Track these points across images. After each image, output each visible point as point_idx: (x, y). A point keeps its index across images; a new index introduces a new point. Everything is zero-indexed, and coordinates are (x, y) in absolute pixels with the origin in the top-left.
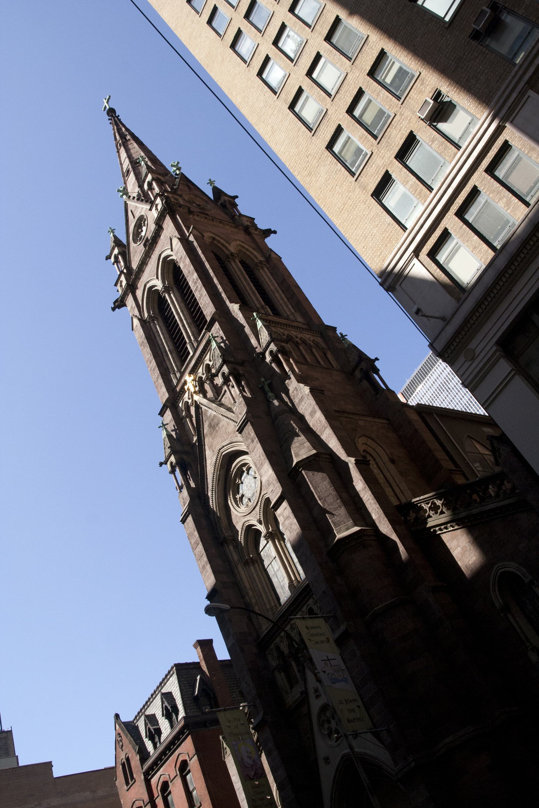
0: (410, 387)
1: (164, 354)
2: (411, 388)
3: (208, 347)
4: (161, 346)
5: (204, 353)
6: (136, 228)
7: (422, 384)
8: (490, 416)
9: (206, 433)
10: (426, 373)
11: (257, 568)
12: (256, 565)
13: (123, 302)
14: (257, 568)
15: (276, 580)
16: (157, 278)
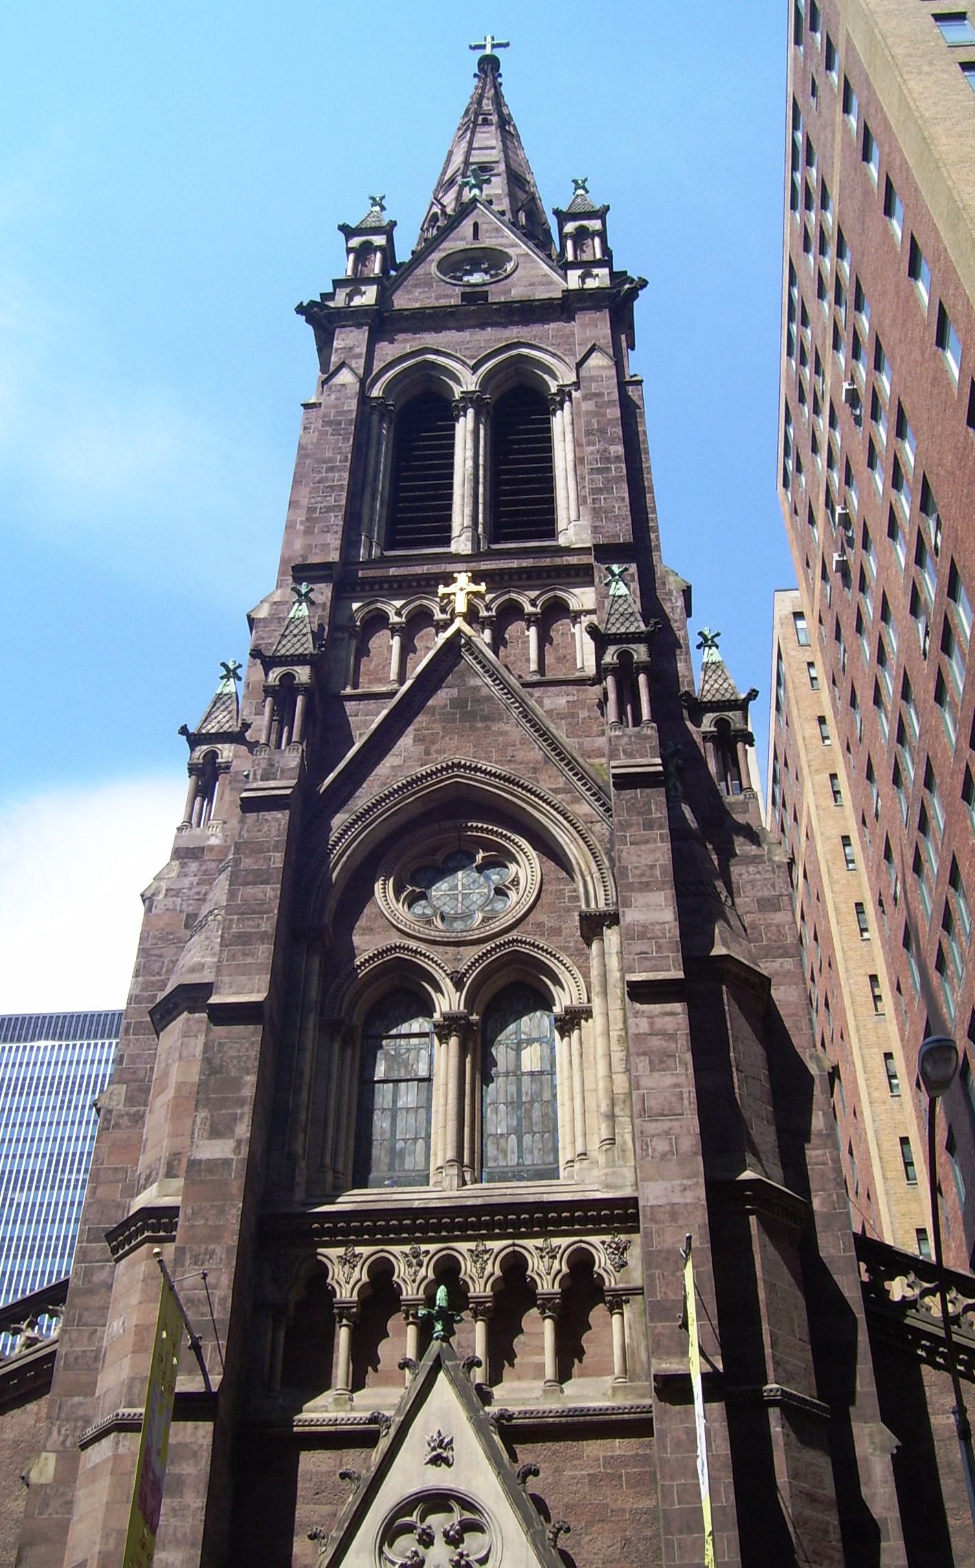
0: (29, 1023)
1: (369, 489)
2: (21, 1029)
3: (549, 577)
4: (371, 470)
5: (529, 578)
6: (463, 255)
7: (57, 1043)
8: (858, 1261)
9: (434, 708)
10: (61, 1034)
11: (349, 1057)
12: (349, 1052)
13: (331, 323)
14: (349, 1057)
15: (386, 1125)
16: (475, 369)
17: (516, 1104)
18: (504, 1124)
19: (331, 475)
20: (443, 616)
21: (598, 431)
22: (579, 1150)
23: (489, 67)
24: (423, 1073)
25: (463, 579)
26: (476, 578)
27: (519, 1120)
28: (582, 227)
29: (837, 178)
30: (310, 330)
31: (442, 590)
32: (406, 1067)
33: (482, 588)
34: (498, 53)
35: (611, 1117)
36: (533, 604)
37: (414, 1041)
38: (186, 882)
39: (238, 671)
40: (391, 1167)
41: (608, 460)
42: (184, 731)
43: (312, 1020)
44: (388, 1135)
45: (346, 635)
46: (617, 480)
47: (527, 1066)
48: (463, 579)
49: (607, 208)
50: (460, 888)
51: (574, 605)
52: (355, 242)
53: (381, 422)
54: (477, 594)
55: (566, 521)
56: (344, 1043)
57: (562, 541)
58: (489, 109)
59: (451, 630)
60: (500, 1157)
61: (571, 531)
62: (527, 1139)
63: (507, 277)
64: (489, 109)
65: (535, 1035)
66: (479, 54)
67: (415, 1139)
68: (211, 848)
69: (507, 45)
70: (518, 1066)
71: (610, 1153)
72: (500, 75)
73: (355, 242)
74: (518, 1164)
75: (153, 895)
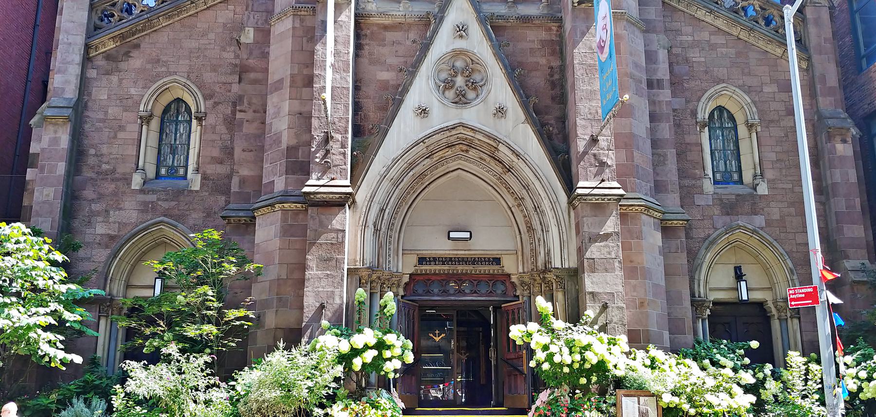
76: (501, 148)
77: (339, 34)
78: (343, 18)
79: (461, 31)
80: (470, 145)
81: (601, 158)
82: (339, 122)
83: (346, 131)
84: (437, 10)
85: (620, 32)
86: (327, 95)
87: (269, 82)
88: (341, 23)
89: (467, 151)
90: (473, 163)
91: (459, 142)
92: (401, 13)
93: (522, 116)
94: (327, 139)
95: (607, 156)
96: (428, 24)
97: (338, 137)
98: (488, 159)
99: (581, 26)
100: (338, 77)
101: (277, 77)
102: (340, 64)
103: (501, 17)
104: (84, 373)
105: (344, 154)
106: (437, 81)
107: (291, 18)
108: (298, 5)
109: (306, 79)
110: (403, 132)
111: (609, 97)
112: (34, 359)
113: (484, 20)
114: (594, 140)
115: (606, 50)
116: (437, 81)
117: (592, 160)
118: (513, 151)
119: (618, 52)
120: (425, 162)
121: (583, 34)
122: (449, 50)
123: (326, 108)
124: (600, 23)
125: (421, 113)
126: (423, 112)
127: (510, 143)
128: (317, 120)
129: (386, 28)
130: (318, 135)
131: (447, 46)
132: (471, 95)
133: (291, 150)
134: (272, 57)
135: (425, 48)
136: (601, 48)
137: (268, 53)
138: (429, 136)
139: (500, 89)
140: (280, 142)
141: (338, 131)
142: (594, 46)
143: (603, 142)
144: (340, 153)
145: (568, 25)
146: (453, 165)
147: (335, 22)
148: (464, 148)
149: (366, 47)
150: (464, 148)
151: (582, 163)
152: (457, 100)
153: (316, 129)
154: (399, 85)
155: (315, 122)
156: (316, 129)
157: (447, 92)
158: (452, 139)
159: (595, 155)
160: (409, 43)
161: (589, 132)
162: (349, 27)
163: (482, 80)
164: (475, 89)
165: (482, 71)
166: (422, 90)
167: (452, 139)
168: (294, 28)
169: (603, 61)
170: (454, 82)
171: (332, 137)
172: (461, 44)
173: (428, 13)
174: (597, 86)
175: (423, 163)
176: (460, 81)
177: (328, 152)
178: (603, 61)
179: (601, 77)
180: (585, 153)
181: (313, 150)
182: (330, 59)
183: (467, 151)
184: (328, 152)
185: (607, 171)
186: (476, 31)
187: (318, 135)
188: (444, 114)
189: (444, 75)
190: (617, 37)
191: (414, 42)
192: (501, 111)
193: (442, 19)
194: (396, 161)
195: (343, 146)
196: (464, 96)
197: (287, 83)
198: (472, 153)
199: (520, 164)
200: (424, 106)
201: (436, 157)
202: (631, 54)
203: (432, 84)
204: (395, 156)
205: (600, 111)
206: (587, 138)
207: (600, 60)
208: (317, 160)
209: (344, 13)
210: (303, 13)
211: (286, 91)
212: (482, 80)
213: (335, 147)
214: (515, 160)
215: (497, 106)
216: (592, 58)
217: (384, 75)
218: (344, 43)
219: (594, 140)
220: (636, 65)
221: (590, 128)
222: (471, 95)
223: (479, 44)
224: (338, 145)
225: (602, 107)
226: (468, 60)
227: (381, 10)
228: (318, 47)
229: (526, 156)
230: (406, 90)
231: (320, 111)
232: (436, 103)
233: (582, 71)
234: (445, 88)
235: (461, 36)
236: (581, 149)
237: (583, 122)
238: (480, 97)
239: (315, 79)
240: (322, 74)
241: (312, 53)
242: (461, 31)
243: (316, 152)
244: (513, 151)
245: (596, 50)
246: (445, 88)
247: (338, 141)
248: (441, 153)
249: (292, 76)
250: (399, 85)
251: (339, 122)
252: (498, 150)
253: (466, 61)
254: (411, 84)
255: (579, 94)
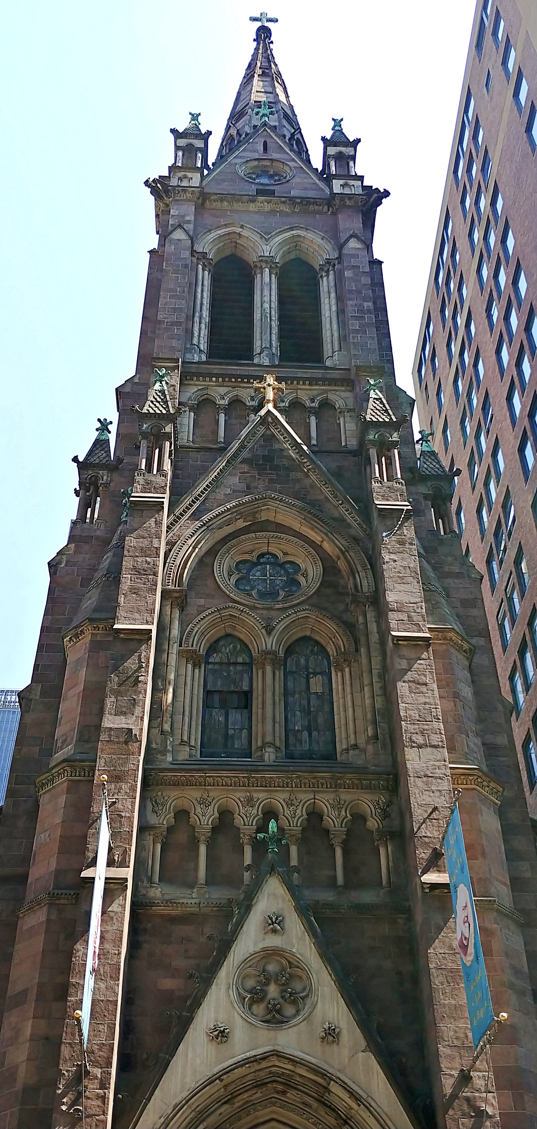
12: (197, 671)
17: (307, 712)
18: (299, 723)
19: (173, 300)
20: (253, 403)
21: (356, 291)
22: (353, 742)
23: (263, 35)
24: (245, 688)
25: (270, 380)
26: (278, 379)
27: (309, 721)
28: (341, 153)
29: (499, 147)
30: (151, 199)
31: (256, 385)
32: (235, 684)
33: (283, 385)
34: (269, 25)
35: (375, 723)
36: (312, 400)
37: (239, 668)
38: (80, 558)
39: (109, 427)
40: (226, 746)
41: (362, 311)
42: (75, 459)
43: (175, 648)
44: (223, 725)
45: (187, 409)
46: (369, 325)
47: (313, 689)
48: (270, 380)
49: (359, 141)
50: (268, 575)
51: (339, 403)
52: (182, 142)
53: (203, 270)
54: (280, 390)
55: (330, 351)
56: (194, 666)
57: (328, 363)
58: (263, 65)
59: (263, 412)
60: (298, 744)
61: (336, 357)
62: (315, 734)
63: (288, 181)
64: (263, 65)
65: (318, 670)
66: (258, 24)
67: (241, 730)
68: (98, 538)
69: (277, 21)
70: (308, 688)
71: (375, 744)
72: (272, 42)
73: (182, 142)
74: (309, 750)
75: (58, 564)
76: (334, 1088)
77: (109, 928)
78: (114, 907)
79: (274, 924)
80: (288, 1083)
81: (478, 1104)
82: (100, 1050)
83: (109, 1064)
84: (242, 897)
85: (487, 925)
86: (85, 1014)
87: (9, 993)
88: (112, 914)
89: (284, 1093)
90: (292, 1111)
91: (270, 1080)
92: (193, 901)
93: (363, 1043)
94: (81, 1075)
95: (486, 1100)
96: (229, 916)
97: (97, 1072)
98: (315, 1104)
99: (437, 919)
100: (102, 985)
101: (19, 987)
102: (107, 968)
103: (328, 905)
104: (148, 386)
105: (104, 1099)
106: (242, 992)
107: (45, 908)
108: (56, 892)
109: (60, 989)
110: (193, 1063)
111: (481, 1014)
112: (157, 516)
113: (303, 910)
114: (465, 1078)
115: (471, 950)
116: (242, 992)
117: (465, 1108)
118: (352, 1094)
119: (488, 952)
120: (222, 1110)
121: (440, 930)
122: (257, 949)
123: (80, 1030)
124: (460, 914)
125: (217, 1037)
126: (220, 1035)
127: (347, 1080)
128: (69, 1048)
129: (173, 920)
130: (67, 1069)
131: (255, 944)
132: (289, 1010)
133: (30, 1092)
134: (16, 959)
135: (225, 946)
136: (464, 948)
137: (12, 954)
138: (227, 1071)
139: (329, 1004)
140: (15, 1080)
141: (95, 1064)
142: (455, 944)
143: (478, 1079)
144: (98, 1097)
145: (419, 917)
146: (264, 1114)
147: (103, 913)
148: (280, 1087)
149: (146, 946)
150: (280, 1087)
151: (451, 1112)
152: (268, 1017)
153: (66, 1061)
154: (188, 997)
155: (65, 1051)
156: (66, 1061)
157: (255, 1007)
158: (262, 1074)
159: (468, 1100)
160: (203, 939)
161: (457, 1064)
162: (123, 919)
163: (304, 989)
164: (294, 1002)
165: (304, 977)
166: (219, 1004)
167: (262, 1074)
168: (48, 921)
169: (468, 964)
170: (265, 993)
171: (87, 1073)
172: (274, 941)
173: (230, 901)
174: (463, 999)
175: (219, 1112)
176: (273, 991)
177: (79, 1095)
178: (468, 964)
179: (467, 988)
180: (454, 1096)
181: (59, 1092)
182: (90, 963)
183: (284, 1093)
184: (80, 1095)
185: (488, 1123)
186: (295, 925)
187: (67, 1069)
188: (249, 1039)
189: (250, 983)
190: (483, 930)
191: (210, 938)
192: (331, 1035)
193: (248, 909)
194: (178, 1108)
195: (104, 1085)
196: (279, 1012)
197: (32, 995)
198: (292, 1095)
199: (361, 1113)
200: (222, 1026)
201: (238, 1102)
202: (507, 955)
203: (233, 994)
204: (177, 1100)
205: (470, 1035)
206: (455, 1073)
207: (464, 964)
208: (64, 1108)
209: (117, 901)
210: (62, 901)
211: (30, 1008)
212: (304, 989)
213: (92, 1088)
214: (354, 1105)
215: (326, 1026)
216: (453, 961)
217: (168, 984)
218: (114, 941)
219: (465, 1078)
220: (517, 971)
221: (458, 1060)
222: (289, 1010)
223: (299, 941)
224: (96, 1083)
225: (472, 1029)
226: (284, 962)
227: (167, 897)
228: (78, 946)
229: (370, 1100)
230: (197, 1003)
231: (73, 1035)
232: (239, 1021)
233: (441, 978)
234: (253, 1001)
235: (274, 931)
236: (448, 1091)
237: (448, 1051)
238: (302, 1013)
239: (72, 990)
240: (81, 982)
241: (70, 954)
242: (274, 924)
243: (64, 1095)
244: (352, 1094)
245: (458, 950)
246: (253, 1001)
247: (96, 1078)
248: (245, 1096)
249: (40, 985)
250: (188, 997)
251: (100, 1050)
252: (329, 1092)
253: (281, 963)
254: (204, 995)
255: (439, 1011)
